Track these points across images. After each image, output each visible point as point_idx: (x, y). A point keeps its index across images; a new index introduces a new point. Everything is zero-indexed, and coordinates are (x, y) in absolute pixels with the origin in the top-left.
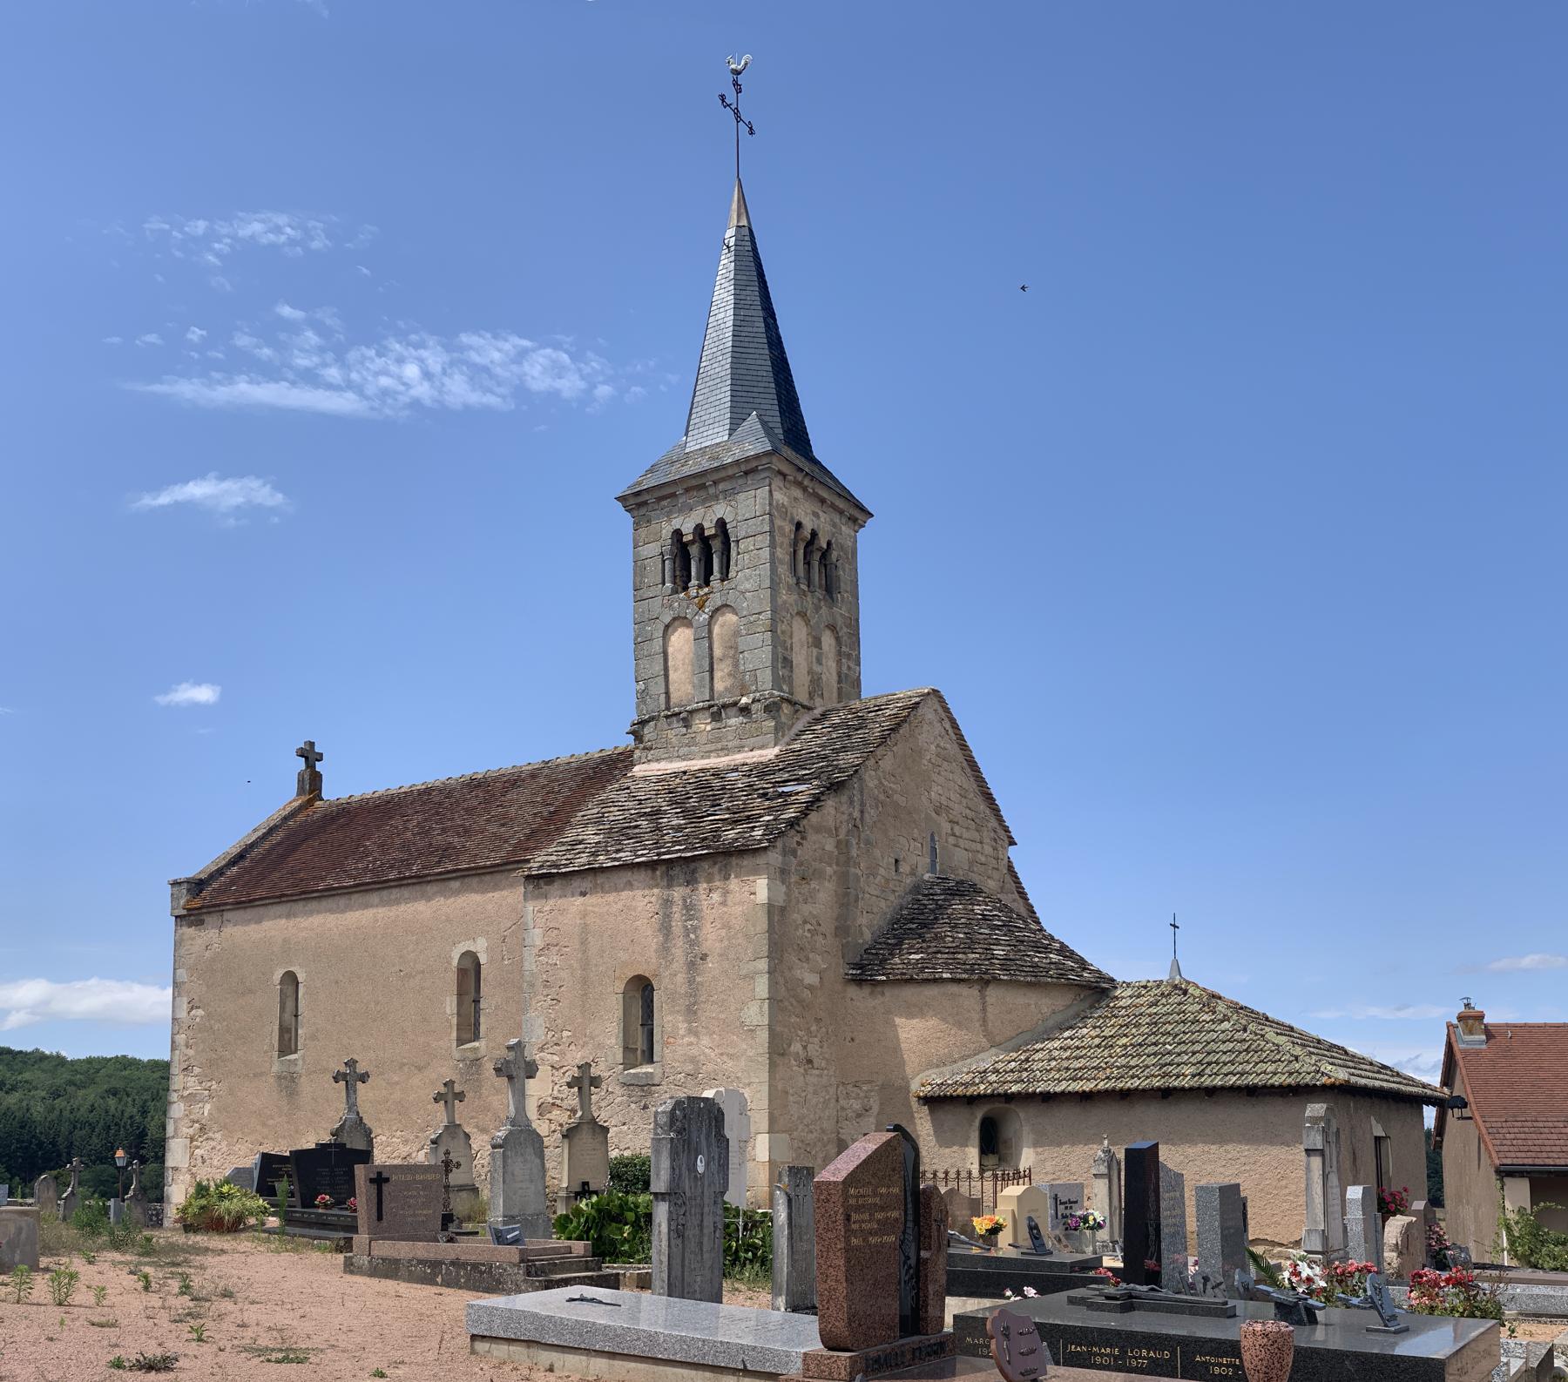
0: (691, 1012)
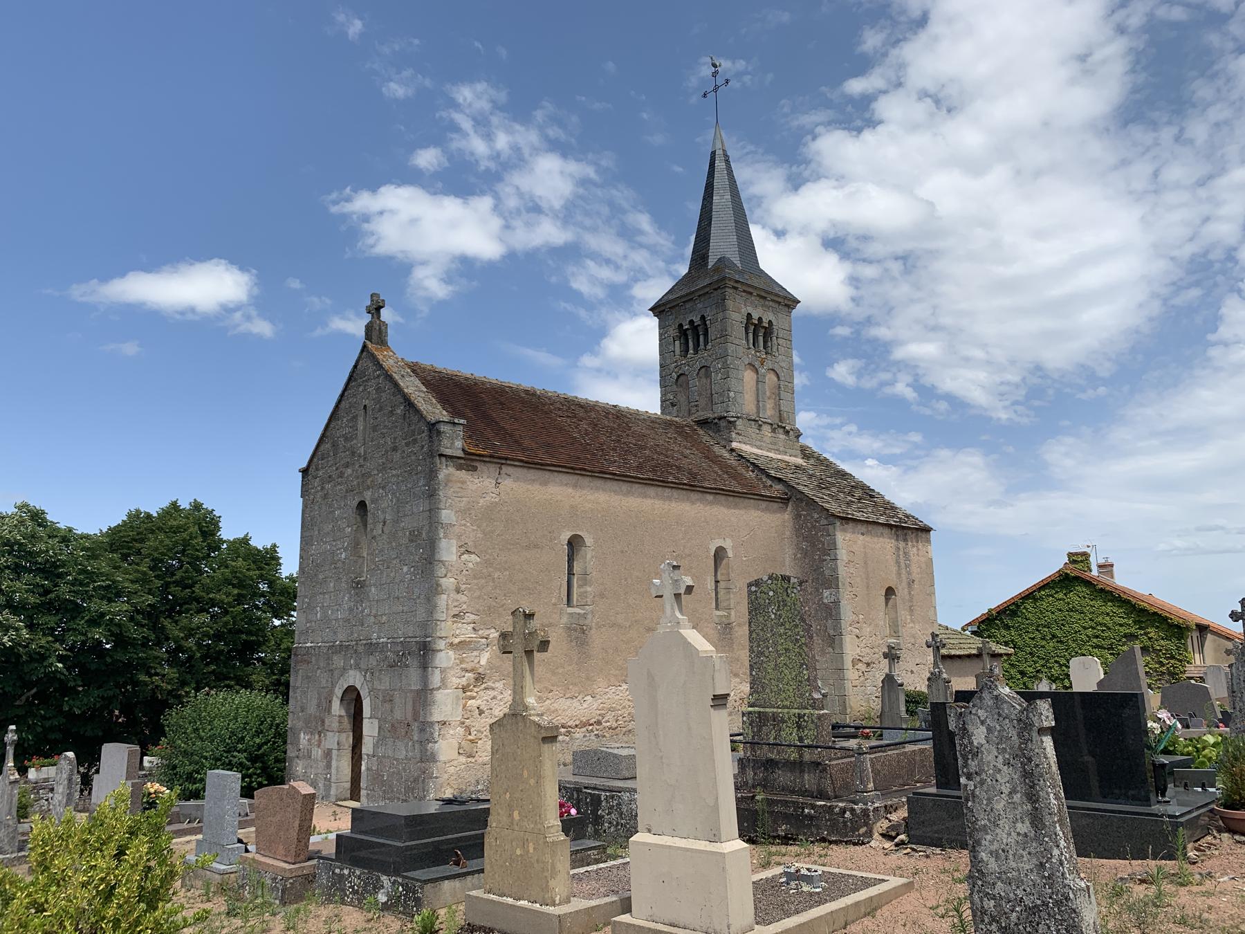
0: (911, 610)
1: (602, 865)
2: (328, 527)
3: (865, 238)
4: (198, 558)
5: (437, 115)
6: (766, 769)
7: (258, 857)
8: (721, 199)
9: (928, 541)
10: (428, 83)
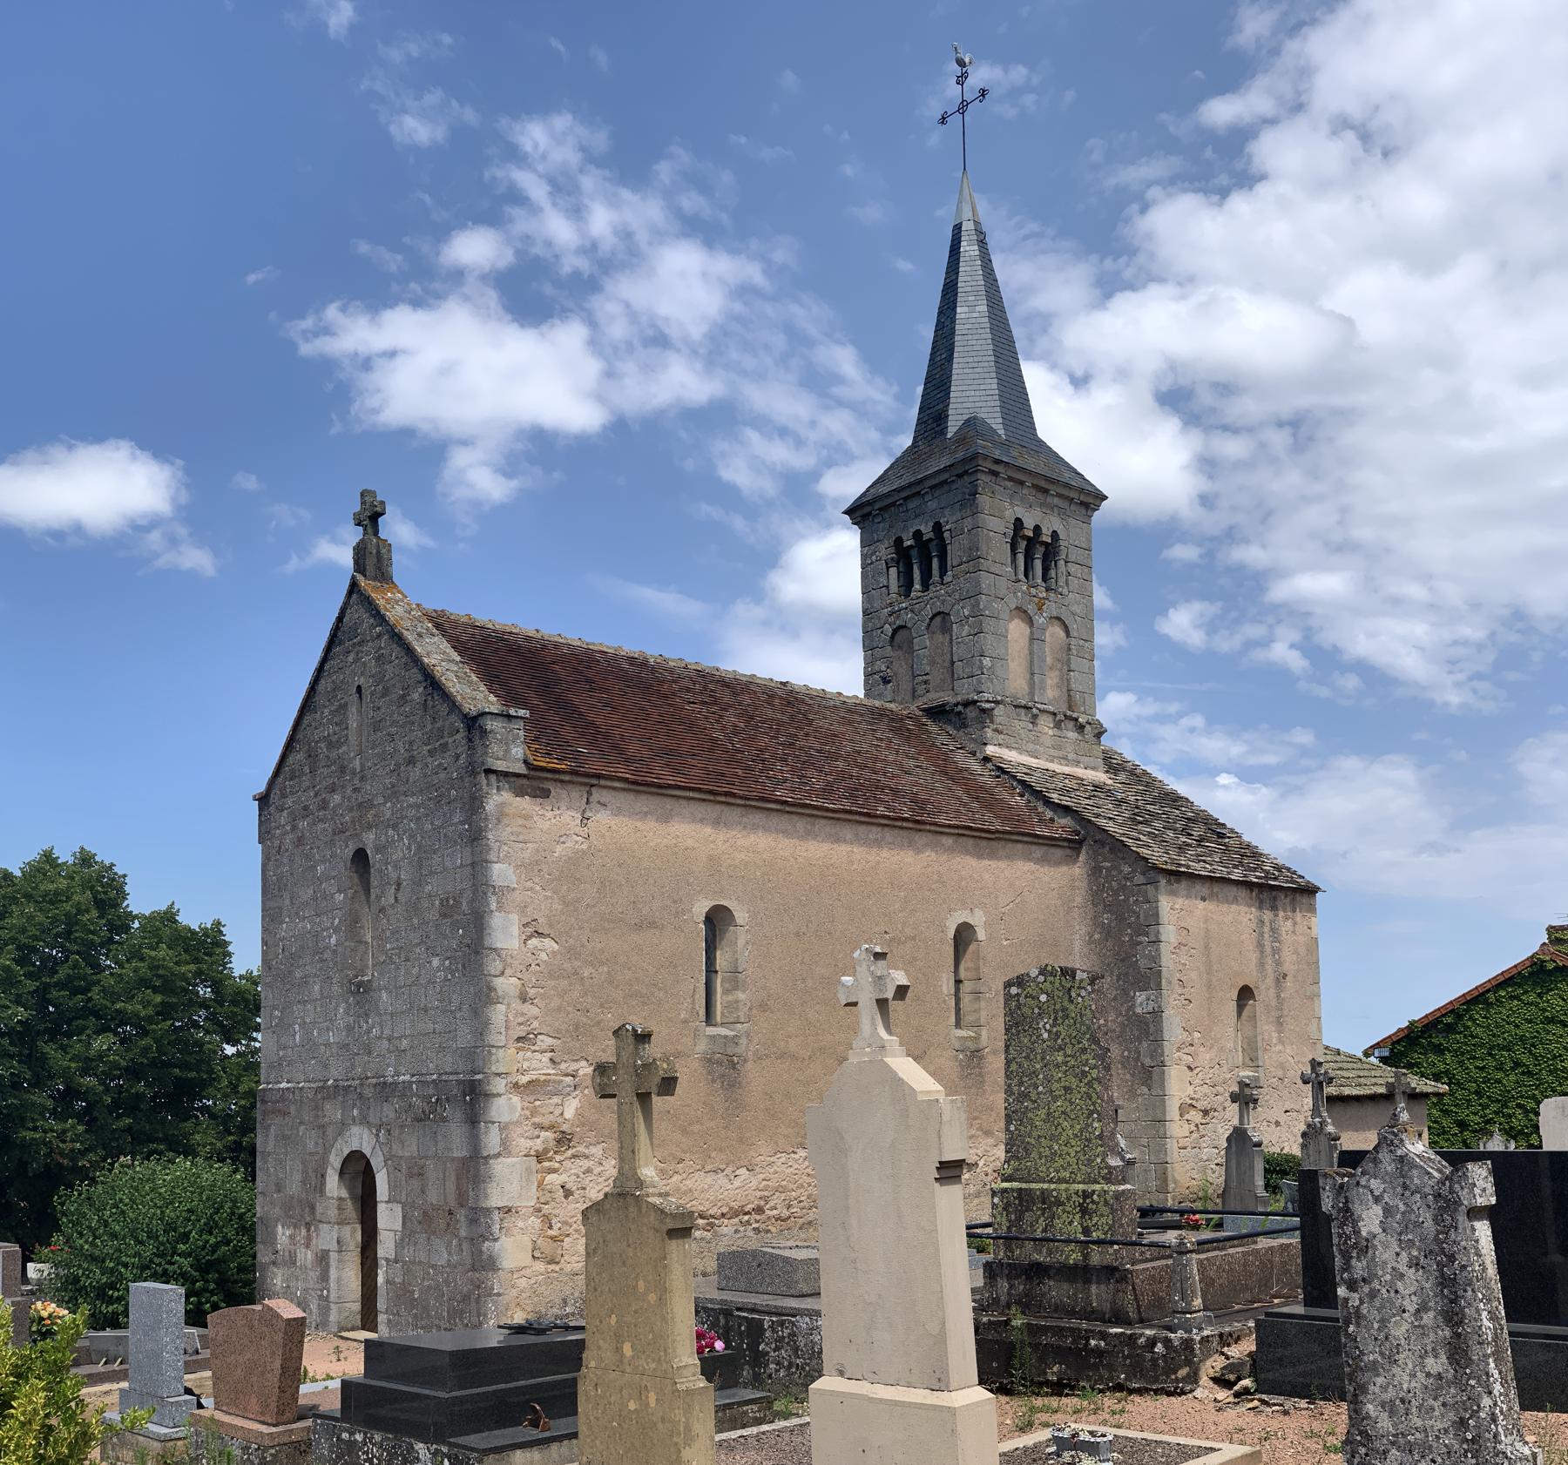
0: (1279, 1022)
1: (765, 1427)
2: (306, 894)
3: (1226, 388)
4: (92, 945)
5: (487, 175)
6: (1029, 1278)
7: (219, 1416)
8: (972, 311)
9: (1312, 909)
10: (470, 116)
